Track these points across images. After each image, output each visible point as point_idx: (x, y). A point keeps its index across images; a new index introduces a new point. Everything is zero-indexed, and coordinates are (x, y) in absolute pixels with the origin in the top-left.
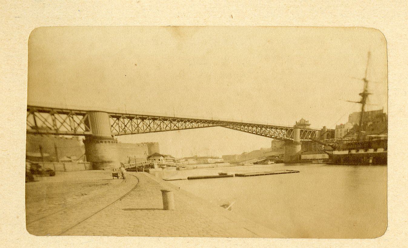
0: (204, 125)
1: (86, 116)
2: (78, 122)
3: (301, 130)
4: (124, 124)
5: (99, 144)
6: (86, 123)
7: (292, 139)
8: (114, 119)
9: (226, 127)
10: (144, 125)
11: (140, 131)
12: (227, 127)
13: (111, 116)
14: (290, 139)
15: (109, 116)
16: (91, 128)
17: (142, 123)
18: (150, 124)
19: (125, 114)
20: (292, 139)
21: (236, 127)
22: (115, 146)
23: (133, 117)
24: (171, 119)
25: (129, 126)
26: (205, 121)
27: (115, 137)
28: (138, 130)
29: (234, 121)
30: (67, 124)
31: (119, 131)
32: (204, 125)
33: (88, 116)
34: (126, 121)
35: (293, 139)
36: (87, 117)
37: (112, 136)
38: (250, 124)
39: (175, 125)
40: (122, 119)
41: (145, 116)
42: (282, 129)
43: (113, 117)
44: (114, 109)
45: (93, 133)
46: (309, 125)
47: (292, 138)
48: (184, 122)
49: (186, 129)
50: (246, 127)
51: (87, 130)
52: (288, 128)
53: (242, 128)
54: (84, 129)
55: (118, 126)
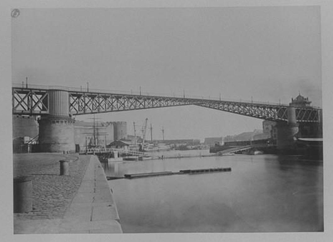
0: (179, 104)
1: (45, 95)
2: (36, 100)
3: (296, 110)
4: (98, 103)
5: (54, 124)
6: (45, 102)
7: (286, 120)
8: (74, 97)
9: (201, 106)
10: (107, 105)
11: (102, 110)
12: (202, 105)
13: (72, 94)
14: (283, 119)
15: (69, 94)
16: (48, 107)
17: (116, 102)
18: (113, 103)
19: (86, 93)
20: (286, 120)
21: (213, 106)
22: (72, 126)
23: (80, 95)
24: (250, 105)
25: (103, 104)
26: (176, 99)
27: (73, 117)
28: (112, 109)
29: (210, 99)
30: (25, 103)
31: (78, 110)
32: (179, 104)
33: (47, 95)
34: (87, 100)
35: (287, 119)
36: (17, 91)
37: (70, 116)
38: (230, 103)
39: (141, 104)
40: (97, 99)
41: (120, 95)
42: (271, 108)
43: (74, 95)
44: (77, 87)
45: (50, 112)
46: (309, 103)
47: (285, 118)
48: (152, 100)
49: (153, 107)
50: (226, 106)
51: (44, 109)
52: (97, 94)
53: (221, 107)
54: (41, 108)
55: (77, 105)
